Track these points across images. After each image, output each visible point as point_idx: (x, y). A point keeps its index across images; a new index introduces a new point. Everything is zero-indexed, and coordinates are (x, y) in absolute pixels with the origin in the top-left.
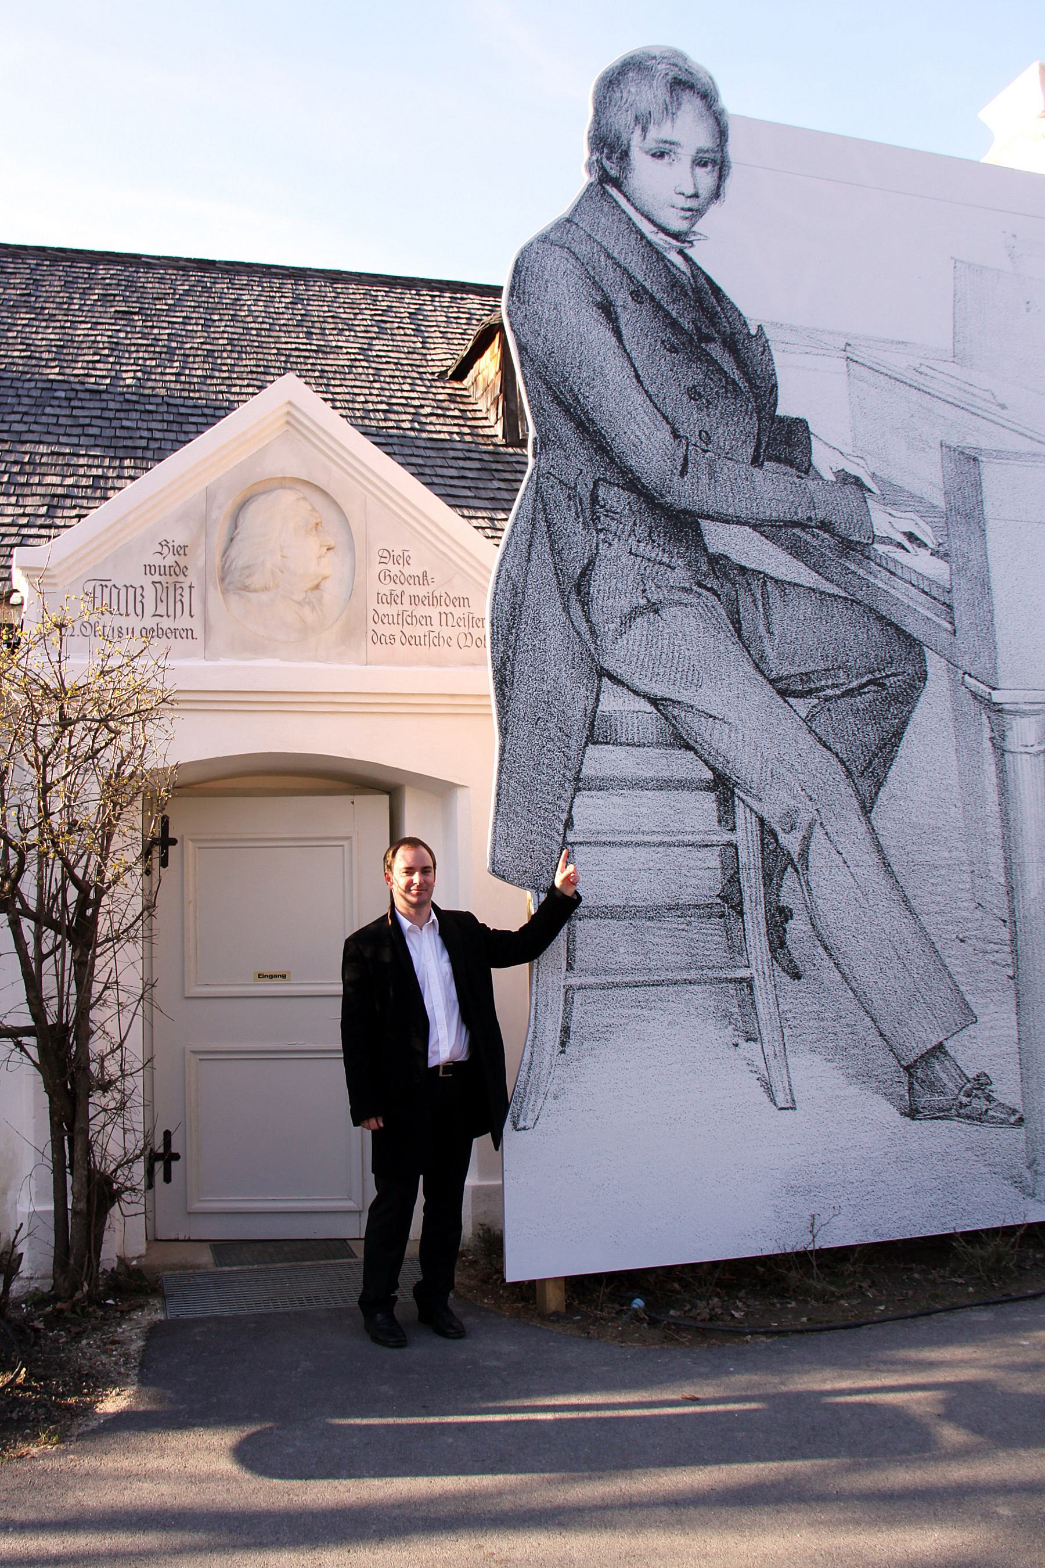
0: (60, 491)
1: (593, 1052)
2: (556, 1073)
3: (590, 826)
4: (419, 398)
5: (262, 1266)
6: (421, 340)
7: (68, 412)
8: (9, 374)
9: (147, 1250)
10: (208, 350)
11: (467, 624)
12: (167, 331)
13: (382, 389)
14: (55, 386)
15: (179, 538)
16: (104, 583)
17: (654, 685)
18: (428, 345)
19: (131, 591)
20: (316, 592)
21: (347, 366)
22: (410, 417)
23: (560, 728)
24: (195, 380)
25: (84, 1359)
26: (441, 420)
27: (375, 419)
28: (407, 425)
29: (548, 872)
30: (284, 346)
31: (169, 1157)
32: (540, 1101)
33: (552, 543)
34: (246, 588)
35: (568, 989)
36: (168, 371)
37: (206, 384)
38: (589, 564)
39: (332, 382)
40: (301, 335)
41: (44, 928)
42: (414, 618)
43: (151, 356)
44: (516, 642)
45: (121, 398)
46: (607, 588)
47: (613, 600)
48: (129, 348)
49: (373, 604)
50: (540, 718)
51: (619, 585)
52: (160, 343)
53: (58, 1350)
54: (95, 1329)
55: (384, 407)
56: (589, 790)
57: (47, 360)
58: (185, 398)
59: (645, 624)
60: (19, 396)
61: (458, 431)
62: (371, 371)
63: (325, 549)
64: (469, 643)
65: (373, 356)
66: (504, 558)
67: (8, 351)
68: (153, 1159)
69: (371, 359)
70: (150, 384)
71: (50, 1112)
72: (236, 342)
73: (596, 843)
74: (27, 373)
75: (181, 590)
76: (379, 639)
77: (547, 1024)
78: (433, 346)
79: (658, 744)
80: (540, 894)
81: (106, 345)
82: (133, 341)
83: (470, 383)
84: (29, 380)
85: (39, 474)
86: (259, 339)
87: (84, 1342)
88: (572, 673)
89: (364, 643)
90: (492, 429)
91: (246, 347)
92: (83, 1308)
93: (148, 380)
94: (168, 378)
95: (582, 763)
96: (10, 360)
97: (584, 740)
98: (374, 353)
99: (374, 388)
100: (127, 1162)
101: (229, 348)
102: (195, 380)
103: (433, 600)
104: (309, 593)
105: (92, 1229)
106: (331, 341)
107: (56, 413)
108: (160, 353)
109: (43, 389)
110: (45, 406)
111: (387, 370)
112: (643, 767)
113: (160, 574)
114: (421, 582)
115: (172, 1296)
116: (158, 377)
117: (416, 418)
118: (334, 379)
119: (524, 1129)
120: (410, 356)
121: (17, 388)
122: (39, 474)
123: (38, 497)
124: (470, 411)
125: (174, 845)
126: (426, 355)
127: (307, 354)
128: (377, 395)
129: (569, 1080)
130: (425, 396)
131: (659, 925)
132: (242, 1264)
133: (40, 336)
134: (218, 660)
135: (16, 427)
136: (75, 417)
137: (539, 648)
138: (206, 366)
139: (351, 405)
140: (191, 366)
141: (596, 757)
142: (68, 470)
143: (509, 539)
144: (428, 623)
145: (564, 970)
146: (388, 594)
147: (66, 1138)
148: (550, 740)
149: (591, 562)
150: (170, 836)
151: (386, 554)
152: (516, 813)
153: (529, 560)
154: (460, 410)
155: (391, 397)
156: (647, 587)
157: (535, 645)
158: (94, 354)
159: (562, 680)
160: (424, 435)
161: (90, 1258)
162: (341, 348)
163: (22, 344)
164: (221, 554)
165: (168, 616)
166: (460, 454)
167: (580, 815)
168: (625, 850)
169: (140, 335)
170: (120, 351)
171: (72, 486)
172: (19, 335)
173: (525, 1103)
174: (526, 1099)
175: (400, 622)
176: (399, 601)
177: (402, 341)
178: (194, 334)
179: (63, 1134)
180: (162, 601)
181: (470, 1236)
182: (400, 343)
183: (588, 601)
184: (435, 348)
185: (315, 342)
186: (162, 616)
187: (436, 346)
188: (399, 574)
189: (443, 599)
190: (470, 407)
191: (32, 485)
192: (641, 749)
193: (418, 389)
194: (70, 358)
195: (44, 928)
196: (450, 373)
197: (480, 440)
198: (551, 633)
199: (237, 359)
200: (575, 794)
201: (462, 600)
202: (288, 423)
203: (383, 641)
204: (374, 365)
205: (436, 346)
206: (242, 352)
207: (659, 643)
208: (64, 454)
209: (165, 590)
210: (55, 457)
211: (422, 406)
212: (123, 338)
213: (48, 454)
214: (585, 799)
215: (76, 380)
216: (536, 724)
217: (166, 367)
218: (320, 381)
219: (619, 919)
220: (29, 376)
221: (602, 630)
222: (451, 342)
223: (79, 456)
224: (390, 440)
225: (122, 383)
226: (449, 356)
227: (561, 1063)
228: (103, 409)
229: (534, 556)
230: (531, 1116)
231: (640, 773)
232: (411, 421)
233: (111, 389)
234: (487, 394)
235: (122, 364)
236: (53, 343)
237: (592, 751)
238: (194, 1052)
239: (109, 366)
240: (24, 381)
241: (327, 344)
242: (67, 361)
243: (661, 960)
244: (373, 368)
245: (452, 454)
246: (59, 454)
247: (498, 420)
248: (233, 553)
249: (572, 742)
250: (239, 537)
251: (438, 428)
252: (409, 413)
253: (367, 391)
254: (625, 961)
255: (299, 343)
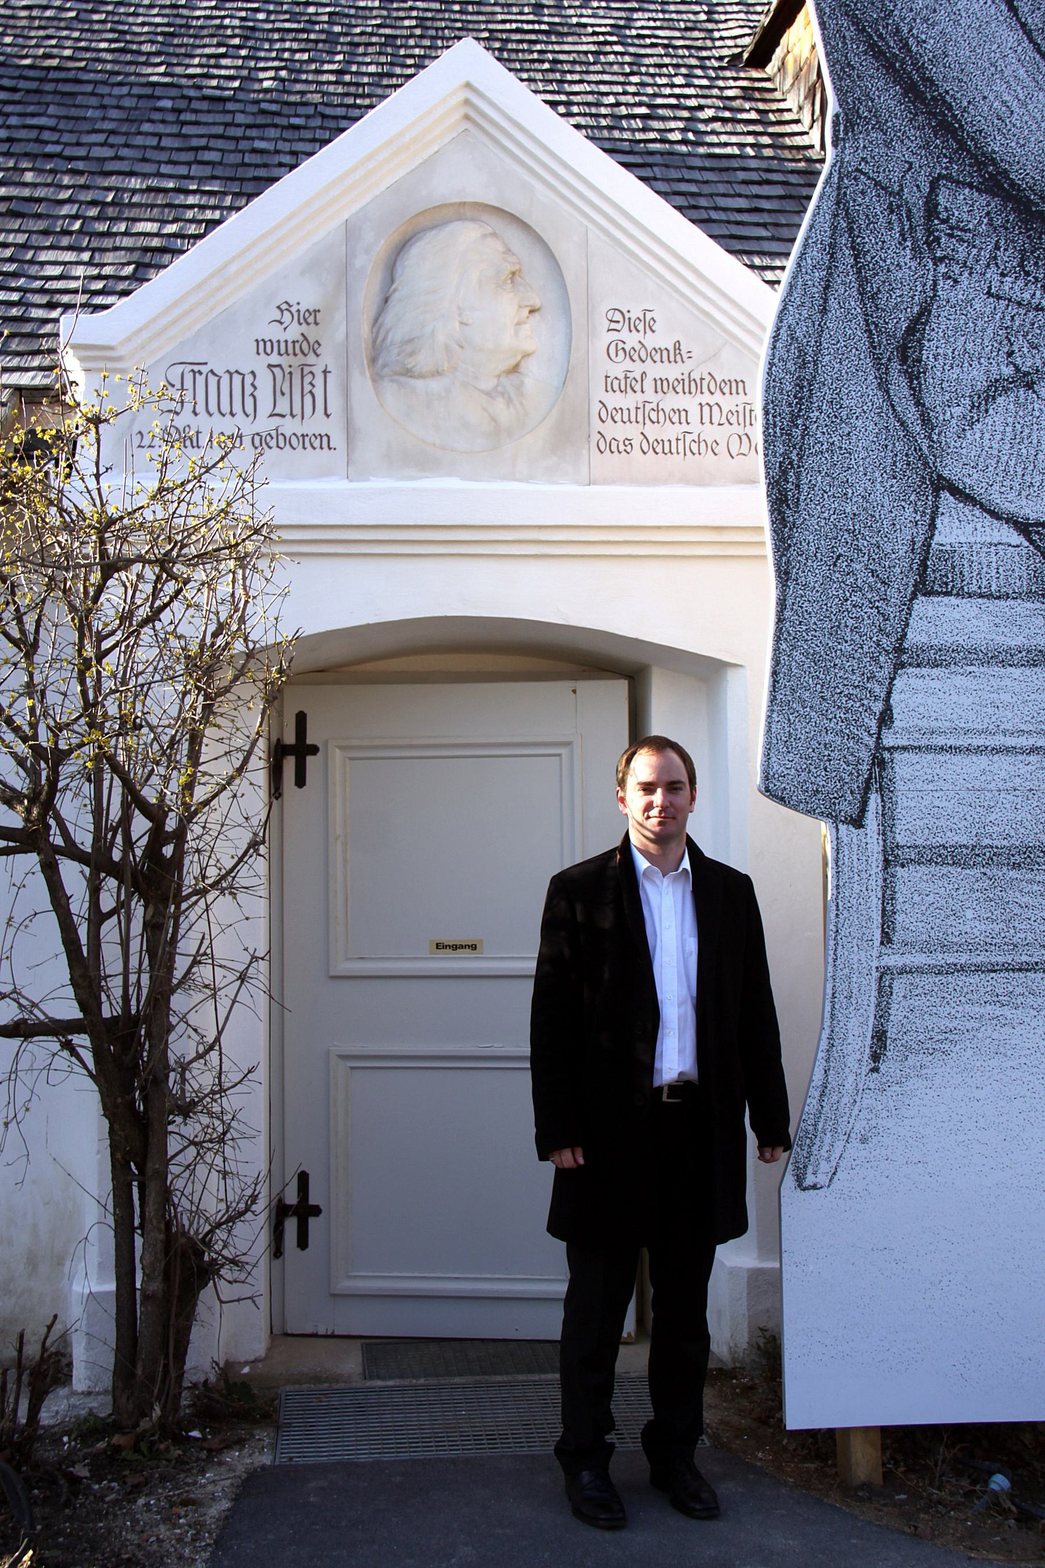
0: (156, 242)
1: (924, 1071)
2: (865, 1102)
3: (920, 723)
4: (696, 96)
5: (432, 1381)
6: (706, 8)
7: (174, 129)
8: (92, 75)
9: (269, 1350)
10: (386, 36)
11: (741, 421)
12: (328, 10)
13: (643, 84)
14: (159, 91)
15: (307, 297)
16: (196, 368)
17: (1024, 502)
18: (716, 17)
19: (237, 379)
20: (512, 377)
21: (592, 53)
22: (681, 125)
23: (872, 572)
24: (366, 80)
25: (133, 1531)
26: (729, 128)
27: (628, 129)
28: (676, 136)
29: (852, 793)
30: (500, 27)
31: (306, 1211)
32: (839, 1145)
33: (862, 281)
34: (408, 373)
35: (884, 972)
36: (326, 67)
37: (381, 86)
38: (921, 314)
39: (569, 77)
40: (526, 10)
41: (103, 875)
42: (661, 413)
43: (303, 46)
44: (803, 438)
45: (254, 109)
46: (949, 352)
47: (958, 370)
48: (270, 35)
49: (598, 392)
50: (840, 555)
51: (970, 346)
52: (317, 27)
53: (100, 1516)
54: (163, 1479)
55: (643, 110)
56: (918, 666)
57: (149, 54)
58: (348, 106)
59: (1012, 406)
60: (103, 107)
61: (754, 141)
62: (627, 59)
63: (526, 312)
64: (745, 449)
65: (632, 37)
66: (785, 308)
67: (91, 41)
68: (280, 1211)
69: (629, 41)
70: (298, 87)
71: (111, 1146)
72: (429, 24)
73: (929, 749)
74: (118, 73)
75: (310, 376)
76: (609, 446)
77: (850, 1026)
78: (723, 17)
79: (1030, 595)
80: (840, 826)
81: (237, 31)
82: (278, 25)
83: (776, 69)
84: (121, 84)
85: (127, 219)
86: (464, 17)
87: (141, 1501)
88: (892, 486)
89: (585, 452)
90: (805, 137)
91: (443, 29)
92: (152, 1444)
93: (296, 81)
94: (325, 78)
95: (907, 625)
96: (94, 55)
97: (911, 589)
98: (634, 32)
99: (630, 84)
100: (226, 1222)
101: (418, 32)
102: (366, 80)
103: (690, 385)
104: (504, 380)
105: (172, 1321)
106: (571, 16)
107: (157, 131)
108: (316, 41)
109: (140, 97)
110: (142, 121)
111: (652, 56)
112: (1005, 630)
113: (280, 354)
114: (672, 358)
115: (290, 1425)
116: (311, 77)
117: (691, 125)
118: (571, 72)
119: (814, 1187)
120: (688, 34)
121: (102, 96)
122: (127, 219)
123: (123, 253)
124: (773, 111)
125: (315, 754)
126: (712, 31)
127: (533, 37)
128: (634, 94)
129: (885, 1114)
130: (706, 92)
131: (1030, 876)
132: (402, 1377)
133: (140, 20)
134: (368, 480)
135: (97, 152)
136: (186, 136)
137: (840, 448)
138: (383, 59)
139: (594, 110)
140: (360, 59)
141: (929, 615)
142: (170, 212)
143: (794, 278)
144: (683, 420)
145: (877, 943)
146: (621, 376)
147: (135, 1183)
148: (856, 589)
149: (925, 311)
150: (309, 741)
151: (618, 317)
152: (802, 702)
153: (824, 311)
154: (758, 111)
155: (655, 95)
156: (1015, 348)
157: (833, 444)
158: (219, 45)
159: (877, 497)
160: (702, 150)
161: (166, 1366)
162: (585, 26)
163: (112, 31)
164: (371, 321)
165: (293, 416)
166: (754, 176)
167: (903, 705)
168: (975, 758)
169: (287, 17)
170: (257, 39)
171: (175, 235)
172: (110, 18)
173: (816, 1147)
174: (817, 1141)
175: (640, 419)
176: (638, 388)
177: (678, 12)
178: (367, 13)
179: (130, 1178)
180: (283, 394)
181: (745, 1346)
182: (674, 16)
183: (919, 373)
184: (726, 21)
185: (546, 19)
186: (283, 416)
187: (728, 17)
188: (638, 347)
189: (705, 383)
190: (775, 106)
191: (116, 234)
192: (1002, 602)
193: (696, 82)
194: (183, 50)
195: (103, 875)
196: (746, 56)
197: (787, 154)
198: (859, 423)
199: (430, 47)
200: (895, 673)
201: (734, 385)
202: (467, 117)
203: (614, 448)
204: (632, 50)
205: (728, 17)
206: (436, 38)
207: (1034, 436)
208: (166, 191)
209: (287, 376)
210: (153, 194)
211: (701, 108)
212: (262, 21)
213: (142, 191)
214: (912, 681)
215: (190, 83)
216: (835, 565)
217: (323, 62)
218: (551, 76)
219: (965, 866)
220: (120, 78)
221: (941, 418)
222: (751, 9)
223: (188, 192)
224: (650, 160)
225: (257, 86)
226: (747, 31)
227: (872, 1086)
228: (226, 125)
229: (833, 304)
230: (824, 1166)
231: (1000, 639)
232: (684, 130)
233: (241, 96)
234: (799, 84)
235: (259, 59)
236: (159, 30)
237: (923, 606)
238: (343, 1057)
239: (240, 62)
240: (114, 85)
241: (563, 21)
242: (177, 55)
243: (1032, 931)
244: (631, 54)
245: (741, 175)
246: (159, 190)
247: (813, 121)
248: (389, 319)
249: (892, 593)
250: (396, 295)
251: (724, 138)
252: (681, 119)
253: (619, 89)
254: (975, 931)
255: (522, 22)
